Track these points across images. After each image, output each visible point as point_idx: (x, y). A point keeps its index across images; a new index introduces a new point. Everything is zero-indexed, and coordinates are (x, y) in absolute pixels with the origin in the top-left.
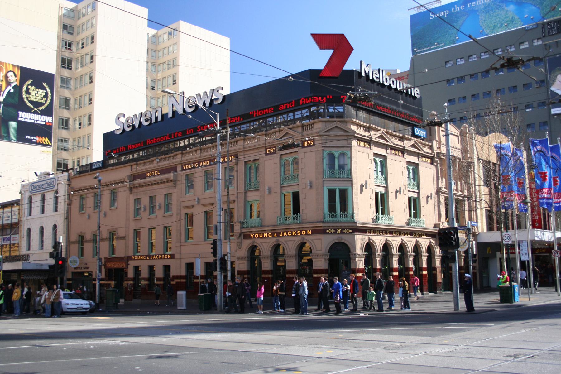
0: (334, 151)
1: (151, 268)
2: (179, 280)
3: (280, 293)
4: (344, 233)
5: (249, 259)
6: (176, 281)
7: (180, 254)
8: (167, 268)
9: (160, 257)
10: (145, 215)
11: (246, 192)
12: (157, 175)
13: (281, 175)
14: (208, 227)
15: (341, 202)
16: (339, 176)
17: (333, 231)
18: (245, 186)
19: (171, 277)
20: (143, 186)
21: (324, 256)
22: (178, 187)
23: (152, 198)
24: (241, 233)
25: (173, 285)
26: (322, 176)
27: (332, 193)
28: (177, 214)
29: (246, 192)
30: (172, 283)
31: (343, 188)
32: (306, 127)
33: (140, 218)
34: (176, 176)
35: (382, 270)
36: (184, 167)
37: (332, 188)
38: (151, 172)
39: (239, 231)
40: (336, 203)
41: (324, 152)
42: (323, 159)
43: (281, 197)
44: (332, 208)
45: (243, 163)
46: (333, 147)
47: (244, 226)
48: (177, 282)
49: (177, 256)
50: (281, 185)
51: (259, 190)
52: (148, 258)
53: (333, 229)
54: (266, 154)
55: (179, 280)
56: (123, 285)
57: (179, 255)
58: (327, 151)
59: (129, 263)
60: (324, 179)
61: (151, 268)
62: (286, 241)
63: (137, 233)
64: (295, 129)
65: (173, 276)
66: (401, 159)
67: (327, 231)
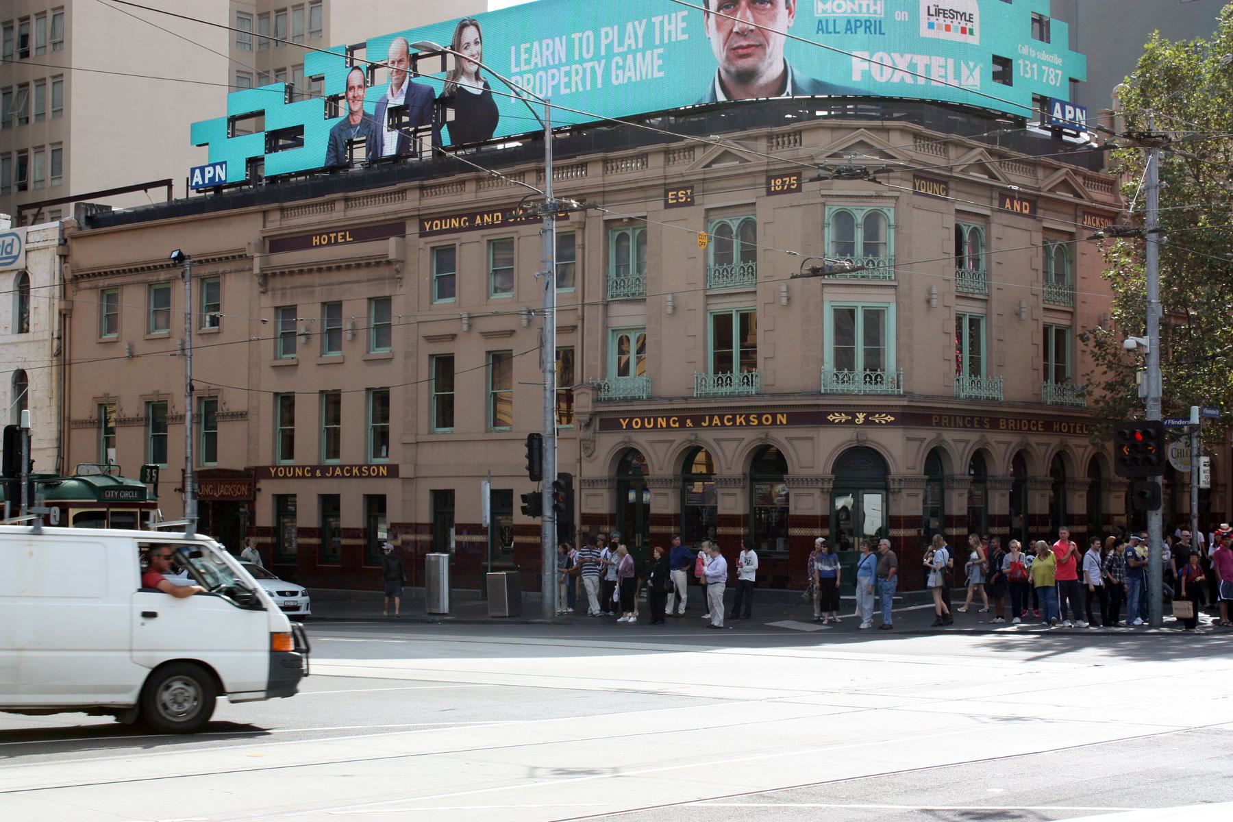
0: (850, 206)
1: (330, 504)
2: (411, 537)
7: (416, 465)
9: (355, 471)
10: (307, 353)
11: (606, 305)
12: (346, 242)
17: (844, 418)
21: (820, 485)
23: (333, 309)
38: (328, 234)
47: (603, 395)
52: (318, 473)
53: (847, 414)
54: (667, 206)
55: (411, 537)
59: (258, 486)
61: (330, 504)
63: (286, 402)
67: (831, 418)
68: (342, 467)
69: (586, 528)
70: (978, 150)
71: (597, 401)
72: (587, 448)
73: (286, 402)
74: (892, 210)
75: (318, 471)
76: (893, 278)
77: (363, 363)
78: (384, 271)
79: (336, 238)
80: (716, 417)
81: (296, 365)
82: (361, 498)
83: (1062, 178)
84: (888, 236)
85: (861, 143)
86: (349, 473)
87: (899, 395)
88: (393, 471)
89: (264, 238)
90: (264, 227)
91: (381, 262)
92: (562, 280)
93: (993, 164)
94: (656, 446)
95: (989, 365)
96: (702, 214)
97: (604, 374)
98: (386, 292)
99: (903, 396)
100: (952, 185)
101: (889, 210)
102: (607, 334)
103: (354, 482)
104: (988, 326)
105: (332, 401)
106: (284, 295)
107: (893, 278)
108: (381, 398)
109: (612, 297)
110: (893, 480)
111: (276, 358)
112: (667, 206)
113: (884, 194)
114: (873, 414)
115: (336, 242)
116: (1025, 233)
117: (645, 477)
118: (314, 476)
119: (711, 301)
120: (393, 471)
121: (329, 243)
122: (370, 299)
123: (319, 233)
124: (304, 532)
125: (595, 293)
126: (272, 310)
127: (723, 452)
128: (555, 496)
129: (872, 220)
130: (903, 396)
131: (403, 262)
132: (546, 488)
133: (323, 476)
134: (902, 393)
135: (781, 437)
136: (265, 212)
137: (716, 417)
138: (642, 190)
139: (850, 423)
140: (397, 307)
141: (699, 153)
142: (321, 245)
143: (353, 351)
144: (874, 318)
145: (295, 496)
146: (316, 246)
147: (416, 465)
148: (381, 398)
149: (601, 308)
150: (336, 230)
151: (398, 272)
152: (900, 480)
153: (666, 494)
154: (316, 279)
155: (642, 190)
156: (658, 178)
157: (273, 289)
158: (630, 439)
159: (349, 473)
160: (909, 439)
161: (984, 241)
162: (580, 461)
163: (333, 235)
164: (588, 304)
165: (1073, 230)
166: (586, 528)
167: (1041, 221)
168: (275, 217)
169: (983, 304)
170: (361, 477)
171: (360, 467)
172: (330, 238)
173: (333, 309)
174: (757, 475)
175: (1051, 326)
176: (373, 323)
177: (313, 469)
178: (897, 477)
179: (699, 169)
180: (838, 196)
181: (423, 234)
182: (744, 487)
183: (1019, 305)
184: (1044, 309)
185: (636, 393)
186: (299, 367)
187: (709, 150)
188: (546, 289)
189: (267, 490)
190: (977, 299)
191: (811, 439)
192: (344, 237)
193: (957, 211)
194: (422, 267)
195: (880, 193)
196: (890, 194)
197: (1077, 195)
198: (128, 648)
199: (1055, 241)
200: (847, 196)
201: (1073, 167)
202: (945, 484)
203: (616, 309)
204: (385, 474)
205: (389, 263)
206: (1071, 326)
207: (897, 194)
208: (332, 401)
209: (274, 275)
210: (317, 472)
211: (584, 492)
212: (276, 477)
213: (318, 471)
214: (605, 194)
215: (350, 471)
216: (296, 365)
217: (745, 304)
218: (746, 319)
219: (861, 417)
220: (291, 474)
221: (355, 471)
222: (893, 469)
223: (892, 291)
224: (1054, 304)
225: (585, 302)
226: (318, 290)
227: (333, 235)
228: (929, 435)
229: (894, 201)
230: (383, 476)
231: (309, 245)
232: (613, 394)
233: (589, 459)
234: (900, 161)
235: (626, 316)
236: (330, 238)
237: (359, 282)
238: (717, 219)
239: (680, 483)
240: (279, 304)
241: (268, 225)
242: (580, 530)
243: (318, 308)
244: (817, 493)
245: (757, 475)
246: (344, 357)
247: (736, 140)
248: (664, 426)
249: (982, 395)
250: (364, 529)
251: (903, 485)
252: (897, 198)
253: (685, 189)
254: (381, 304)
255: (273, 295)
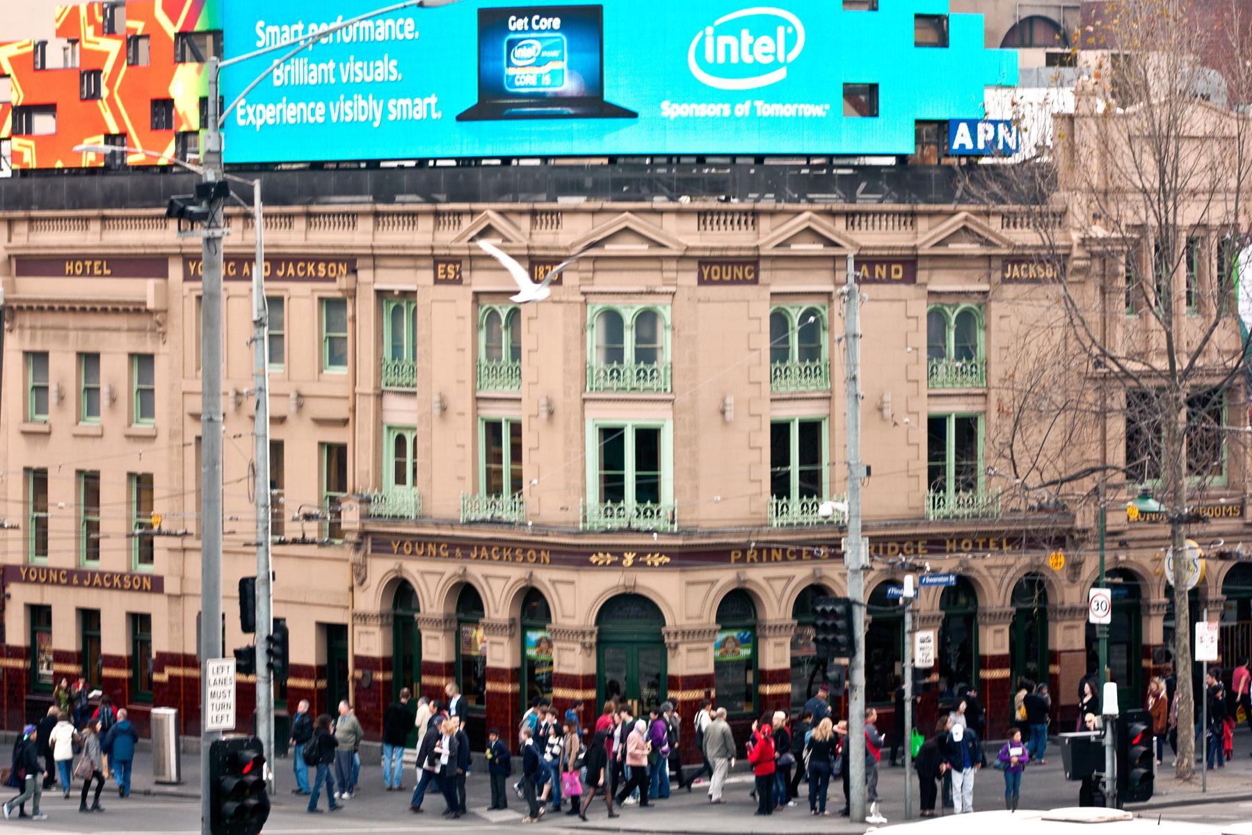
0: (618, 304)
1: (89, 619)
2: (178, 672)
3: (30, 697)
4: (644, 564)
5: (391, 620)
6: (169, 671)
7: (182, 578)
8: (140, 624)
9: (116, 580)
10: (61, 419)
11: (380, 395)
12: (102, 275)
13: (475, 359)
14: (331, 339)
15: (639, 467)
16: (635, 384)
17: (609, 559)
18: (379, 374)
19: (154, 656)
20: (51, 309)
21: (580, 639)
22: (174, 336)
23: (90, 360)
24: (364, 534)
25: (160, 684)
26: (577, 385)
27: (611, 438)
28: (172, 435)
29: (380, 395)
30: (156, 677)
31: (647, 421)
32: (544, 217)
33: (45, 428)
34: (165, 293)
35: (892, 689)
36: (192, 268)
37: (612, 421)
38: (83, 261)
39: (357, 526)
40: (623, 469)
41: (589, 307)
42: (583, 331)
43: (475, 430)
44: (612, 490)
45: (372, 295)
46: (618, 293)
47: (373, 509)
48: (171, 677)
49: (170, 586)
50: (474, 390)
51: (414, 394)
52: (75, 581)
53: (612, 554)
54: (437, 281)
55: (178, 672)
56: (158, 705)
57: (177, 580)
58: (599, 307)
59: (7, 591)
60: (585, 396)
61: (89, 619)
62: (486, 577)
63: (38, 479)
64: (515, 218)
65: (160, 655)
66: (905, 290)
67: (594, 559)
68: (102, 574)
69: (359, 674)
70: (806, 215)
71: (365, 516)
72: (359, 574)
73: (38, 479)
74: (669, 308)
75: (75, 578)
76: (669, 390)
77: (124, 440)
78: (146, 322)
79: (92, 267)
80: (484, 549)
81: (48, 434)
82: (124, 615)
83: (961, 225)
84: (665, 339)
85: (627, 230)
86: (111, 582)
87: (672, 534)
88: (156, 585)
89: (10, 257)
90: (10, 240)
91: (137, 309)
92: (336, 358)
93: (825, 226)
94: (428, 577)
95: (832, 482)
96: (470, 297)
97: (378, 484)
98: (147, 348)
99: (677, 534)
100: (762, 265)
101: (664, 308)
102: (382, 431)
103: (116, 595)
104: (831, 430)
105: (90, 482)
106: (33, 338)
107: (669, 390)
108: (142, 484)
109: (387, 385)
110: (668, 634)
111: (26, 420)
112: (437, 281)
113: (657, 290)
114: (645, 554)
115: (92, 275)
116: (896, 305)
117: (417, 616)
118: (69, 584)
119: (481, 404)
120: (156, 585)
121: (83, 274)
122: (131, 355)
123: (73, 258)
124: (61, 657)
125: (367, 384)
126: (20, 356)
127: (491, 590)
128: (269, 652)
129: (647, 318)
130: (677, 534)
131: (166, 311)
132: (258, 640)
133: (80, 585)
134: (676, 530)
135: (545, 577)
136: (11, 222)
137: (484, 549)
138: (409, 258)
139: (617, 564)
140: (160, 365)
141: (466, 222)
142: (74, 275)
143: (111, 421)
144: (648, 440)
145: (917, 44)
146: (69, 275)
147: (182, 578)
148: (142, 484)
149: (372, 399)
150: (93, 258)
151: (160, 324)
152: (676, 634)
153: (436, 638)
154: (71, 321)
155: (409, 258)
156: (425, 248)
157: (21, 327)
158: (400, 566)
159: (111, 582)
160: (689, 584)
161: (827, 323)
162: (352, 589)
163: (88, 263)
164: (361, 394)
165: (985, 287)
166: (359, 674)
167: (925, 285)
168: (21, 229)
169: (825, 403)
170: (122, 589)
171: (122, 577)
172: (85, 267)
173: (90, 360)
174: (528, 622)
175: (950, 416)
176: (136, 386)
177: (70, 574)
178: (673, 630)
179: (464, 243)
180: (601, 293)
181: (187, 277)
182: (511, 636)
183: (881, 398)
184: (929, 396)
185: (404, 511)
186: (53, 436)
187: (477, 219)
188: (257, 408)
189: (20, 596)
190: (813, 399)
191: (572, 583)
192: (101, 267)
193: (773, 294)
194: (185, 318)
195: (653, 289)
196: (664, 289)
197: (988, 243)
198: (1224, 203)
199: (957, 306)
200: (613, 293)
201: (973, 208)
202: (758, 631)
203: (391, 402)
204: (149, 587)
205: (149, 312)
206: (985, 412)
207: (673, 289)
208: (90, 482)
209: (20, 309)
210: (74, 578)
211: (357, 628)
212: (27, 581)
213: (75, 578)
214: (376, 259)
215: (110, 579)
216: (48, 434)
217: (809, 411)
218: (516, 429)
219: (629, 558)
220: (46, 577)
221: (116, 580)
222: (668, 621)
223: (669, 406)
224: (953, 388)
225: (358, 390)
226: (72, 334)
227: (88, 263)
228: (724, 577)
229: (671, 297)
230: (146, 590)
231: (60, 273)
232: (388, 510)
233: (362, 589)
234: (672, 249)
235: (400, 411)
236: (85, 267)
237: (118, 330)
238: (486, 304)
239: (454, 625)
240: (28, 347)
241: (13, 238)
242: (353, 677)
243: (72, 359)
244: (578, 648)
245: (528, 622)
246: (102, 429)
247: (501, 213)
248: (434, 553)
249: (810, 521)
250: (129, 657)
251: (679, 638)
252: (674, 294)
253: (455, 263)
254: (144, 361)
255: (21, 335)
